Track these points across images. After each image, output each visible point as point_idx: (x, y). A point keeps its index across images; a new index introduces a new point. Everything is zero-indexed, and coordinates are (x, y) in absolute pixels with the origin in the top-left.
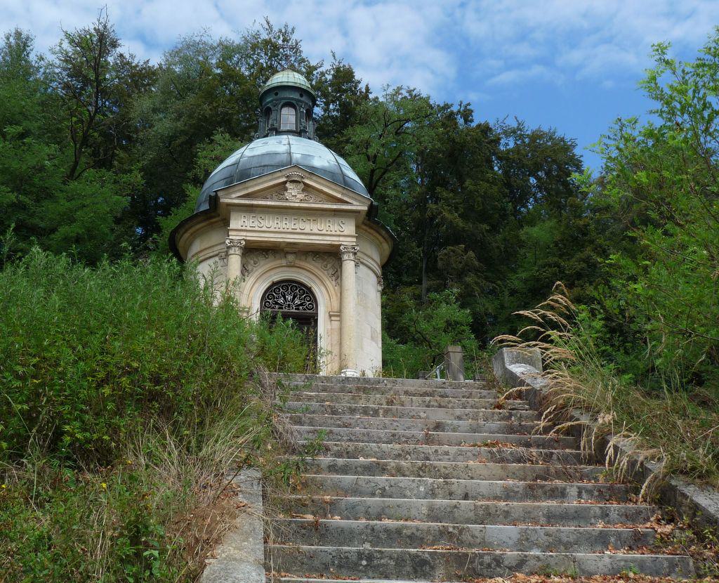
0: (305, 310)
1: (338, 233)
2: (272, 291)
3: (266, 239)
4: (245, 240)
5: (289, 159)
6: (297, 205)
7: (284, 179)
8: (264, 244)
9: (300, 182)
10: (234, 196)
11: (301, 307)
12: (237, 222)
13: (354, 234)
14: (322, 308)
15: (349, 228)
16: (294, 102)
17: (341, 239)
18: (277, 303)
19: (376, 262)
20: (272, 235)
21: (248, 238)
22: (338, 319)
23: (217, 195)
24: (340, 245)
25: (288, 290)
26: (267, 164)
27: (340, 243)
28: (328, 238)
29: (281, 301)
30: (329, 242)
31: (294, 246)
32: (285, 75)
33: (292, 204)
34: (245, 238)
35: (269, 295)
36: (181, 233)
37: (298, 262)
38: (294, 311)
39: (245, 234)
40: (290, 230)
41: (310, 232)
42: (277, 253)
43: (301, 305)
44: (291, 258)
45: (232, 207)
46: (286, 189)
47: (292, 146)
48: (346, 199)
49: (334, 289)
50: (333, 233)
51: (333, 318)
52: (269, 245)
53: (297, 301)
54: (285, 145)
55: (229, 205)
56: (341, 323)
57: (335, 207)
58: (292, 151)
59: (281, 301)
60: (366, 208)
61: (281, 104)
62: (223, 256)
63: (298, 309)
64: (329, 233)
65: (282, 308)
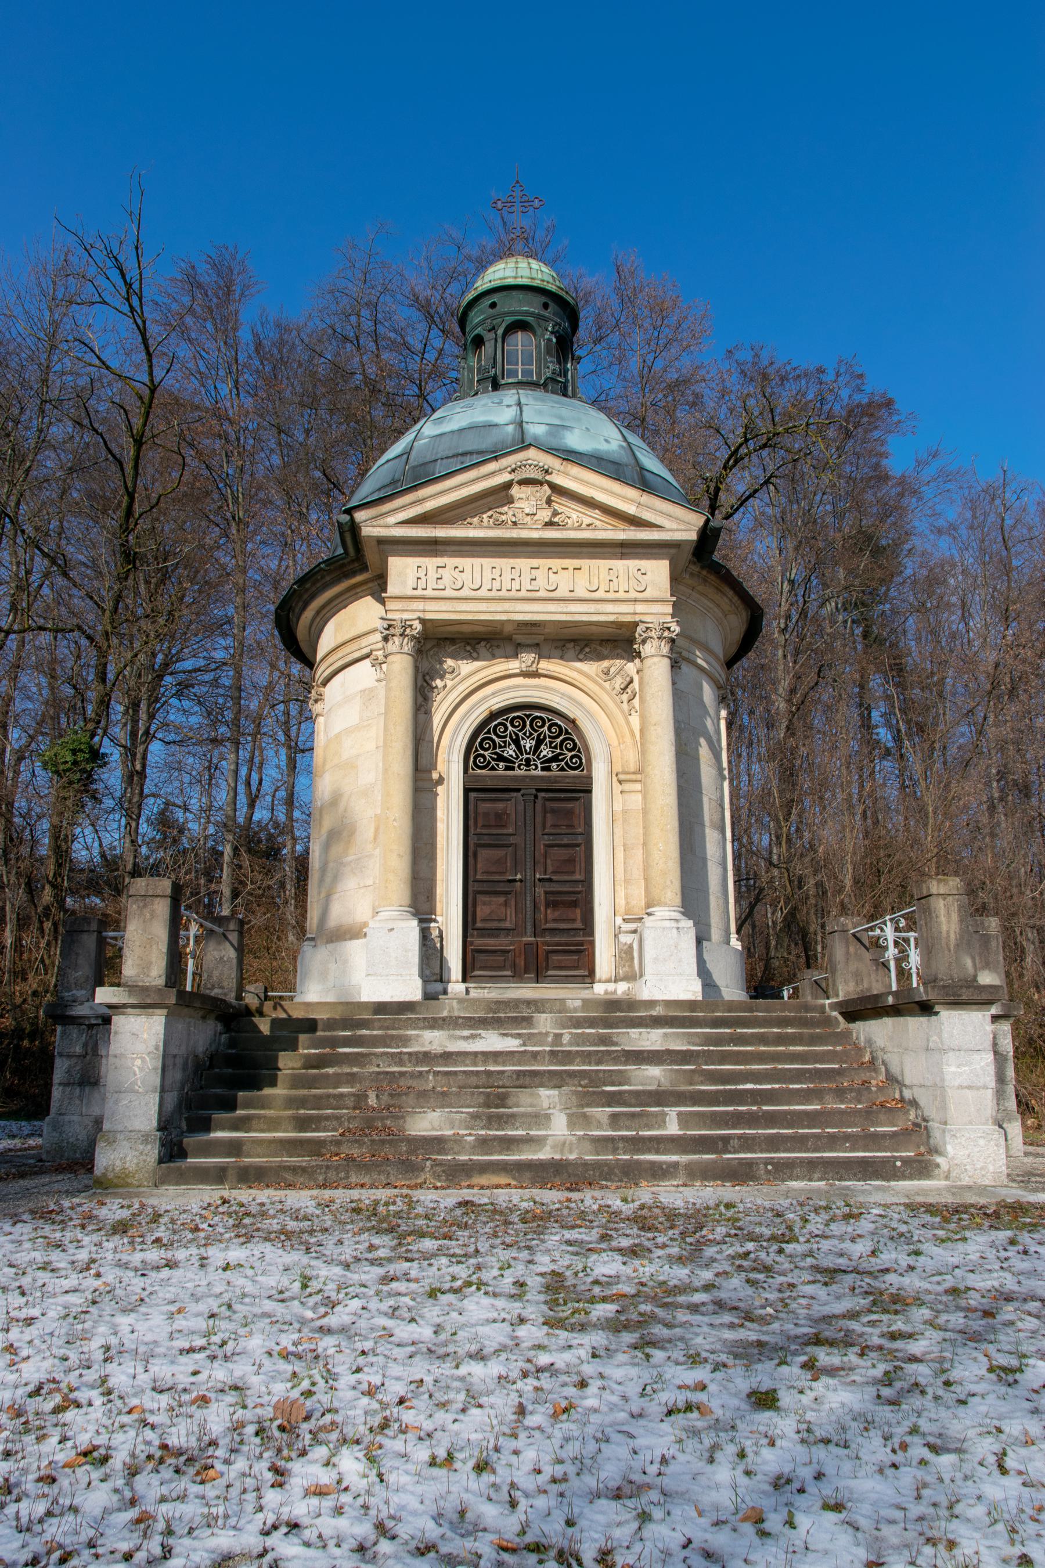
0: (562, 769)
1: (633, 595)
2: (489, 732)
3: (469, 617)
4: (423, 621)
5: (518, 436)
6: (535, 535)
7: (506, 477)
8: (465, 629)
9: (541, 483)
10: (392, 520)
11: (554, 765)
12: (404, 572)
13: (667, 594)
14: (315, 906)
15: (657, 573)
16: (529, 319)
17: (640, 608)
18: (501, 758)
19: (716, 657)
20: (482, 606)
21: (429, 616)
22: (638, 786)
23: (352, 519)
24: (636, 624)
25: (524, 726)
26: (469, 448)
27: (637, 618)
28: (610, 608)
29: (510, 751)
30: (612, 618)
31: (535, 630)
32: (512, 265)
33: (525, 534)
34: (421, 615)
35: (483, 740)
36: (297, 610)
37: (545, 665)
38: (539, 773)
39: (420, 605)
40: (523, 594)
41: (568, 595)
42: (495, 643)
43: (555, 759)
44: (527, 658)
45: (386, 547)
46: (510, 501)
47: (525, 408)
48: (647, 516)
49: (454, 687)
50: (621, 595)
51: (627, 787)
52: (476, 629)
53: (546, 752)
54: (508, 406)
55: (381, 541)
56: (645, 798)
57: (621, 536)
58: (525, 418)
59: (510, 751)
60: (693, 536)
61: (504, 326)
62: (381, 658)
63: (548, 769)
64: (611, 596)
65: (513, 769)
